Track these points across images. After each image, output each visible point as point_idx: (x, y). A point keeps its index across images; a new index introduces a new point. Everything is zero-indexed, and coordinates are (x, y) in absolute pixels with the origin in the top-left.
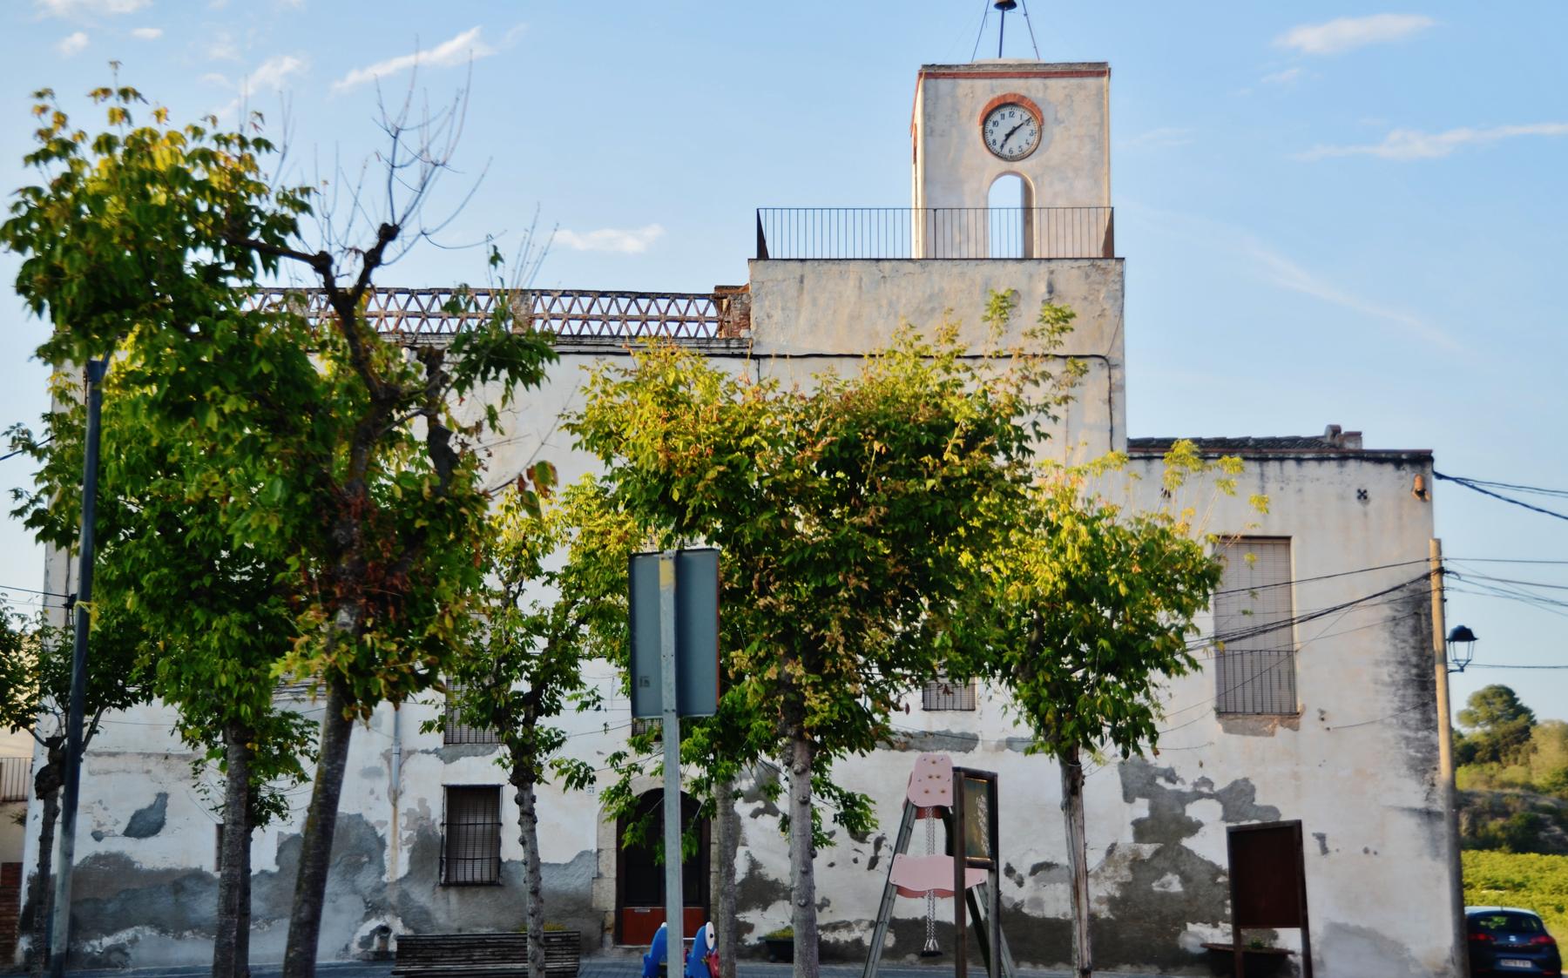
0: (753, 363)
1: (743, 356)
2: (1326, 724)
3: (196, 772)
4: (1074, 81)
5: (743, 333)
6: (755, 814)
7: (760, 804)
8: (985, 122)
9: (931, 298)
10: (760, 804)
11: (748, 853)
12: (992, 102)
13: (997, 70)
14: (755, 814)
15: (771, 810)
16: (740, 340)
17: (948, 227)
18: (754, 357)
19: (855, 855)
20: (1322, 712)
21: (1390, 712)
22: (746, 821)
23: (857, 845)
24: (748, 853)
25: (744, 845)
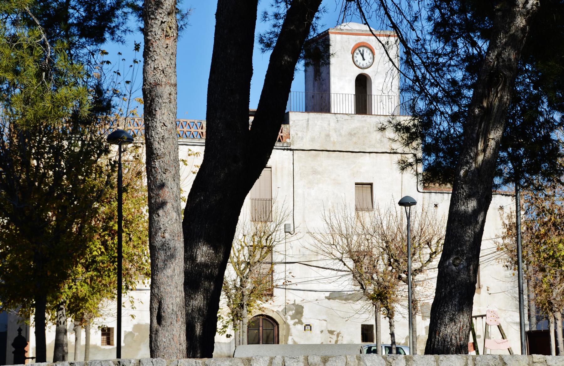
0: (292, 152)
1: (288, 150)
2: (489, 292)
3: (137, 62)
4: (116, 315)
5: (288, 140)
6: (294, 324)
7: (297, 320)
8: (353, 54)
9: (336, 132)
10: (297, 320)
11: (292, 338)
12: (355, 46)
13: (358, 32)
14: (294, 324)
15: (300, 322)
16: (287, 143)
17: (336, 106)
18: (291, 150)
19: (330, 339)
20: (488, 288)
21: (510, 288)
22: (292, 327)
23: (331, 336)
24: (292, 338)
25: (291, 336)
